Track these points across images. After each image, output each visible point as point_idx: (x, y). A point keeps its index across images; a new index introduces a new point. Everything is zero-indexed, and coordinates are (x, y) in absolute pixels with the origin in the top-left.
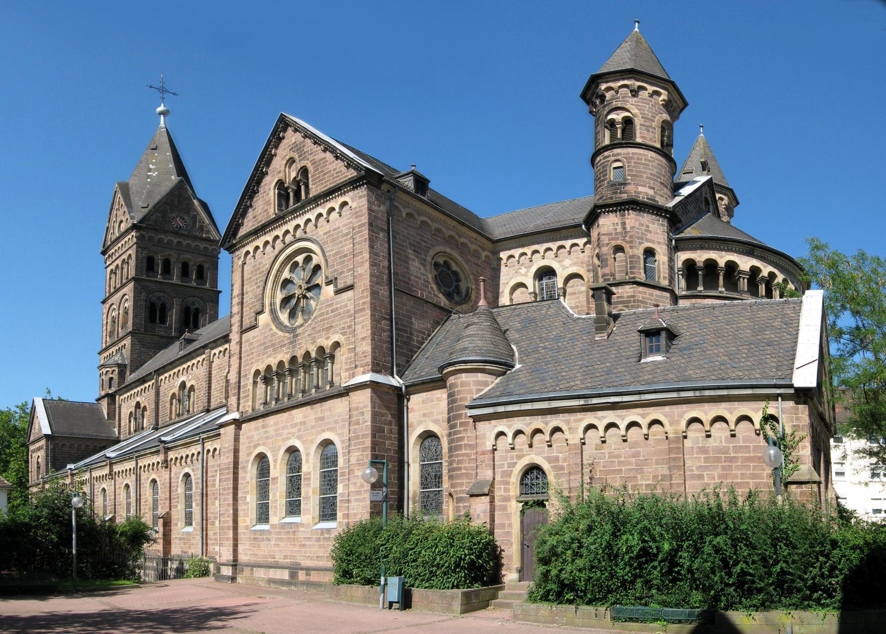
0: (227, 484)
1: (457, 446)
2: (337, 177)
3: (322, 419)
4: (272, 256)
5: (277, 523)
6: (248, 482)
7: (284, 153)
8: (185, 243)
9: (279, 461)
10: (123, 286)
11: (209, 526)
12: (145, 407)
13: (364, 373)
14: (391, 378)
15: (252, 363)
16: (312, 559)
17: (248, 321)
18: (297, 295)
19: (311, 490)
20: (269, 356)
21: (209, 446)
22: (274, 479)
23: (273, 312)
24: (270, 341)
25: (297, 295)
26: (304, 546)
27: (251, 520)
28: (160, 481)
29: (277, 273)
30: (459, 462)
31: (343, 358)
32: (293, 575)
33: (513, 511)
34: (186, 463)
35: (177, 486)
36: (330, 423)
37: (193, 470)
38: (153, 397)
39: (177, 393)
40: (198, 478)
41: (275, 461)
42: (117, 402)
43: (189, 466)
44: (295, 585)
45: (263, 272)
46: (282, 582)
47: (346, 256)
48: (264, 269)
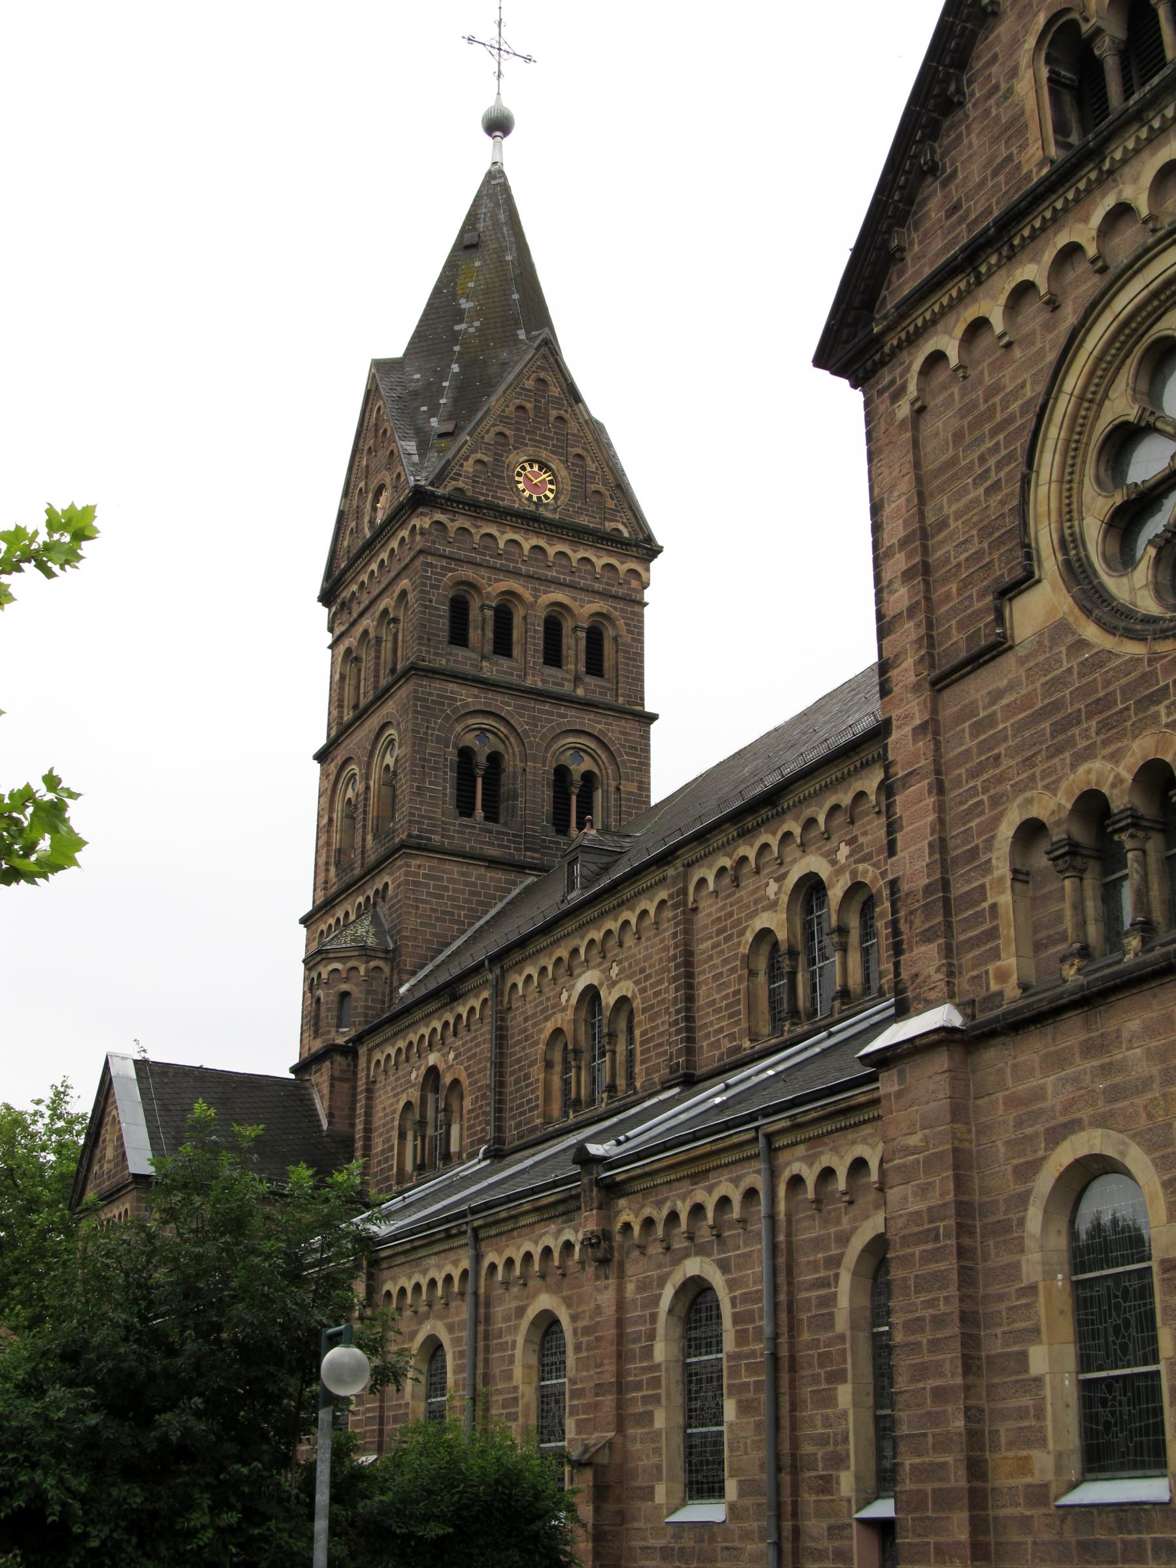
0: (931, 1303)
6: (1032, 1289)
8: (551, 551)
10: (382, 695)
11: (809, 1498)
12: (456, 1082)
15: (996, 801)
20: (1087, 754)
27: (1059, 1456)
28: (574, 1318)
29: (1078, 407)
34: (691, 1237)
35: (652, 1336)
37: (724, 1266)
38: (486, 1049)
39: (568, 1029)
42: (362, 1075)
48: (1015, 406)
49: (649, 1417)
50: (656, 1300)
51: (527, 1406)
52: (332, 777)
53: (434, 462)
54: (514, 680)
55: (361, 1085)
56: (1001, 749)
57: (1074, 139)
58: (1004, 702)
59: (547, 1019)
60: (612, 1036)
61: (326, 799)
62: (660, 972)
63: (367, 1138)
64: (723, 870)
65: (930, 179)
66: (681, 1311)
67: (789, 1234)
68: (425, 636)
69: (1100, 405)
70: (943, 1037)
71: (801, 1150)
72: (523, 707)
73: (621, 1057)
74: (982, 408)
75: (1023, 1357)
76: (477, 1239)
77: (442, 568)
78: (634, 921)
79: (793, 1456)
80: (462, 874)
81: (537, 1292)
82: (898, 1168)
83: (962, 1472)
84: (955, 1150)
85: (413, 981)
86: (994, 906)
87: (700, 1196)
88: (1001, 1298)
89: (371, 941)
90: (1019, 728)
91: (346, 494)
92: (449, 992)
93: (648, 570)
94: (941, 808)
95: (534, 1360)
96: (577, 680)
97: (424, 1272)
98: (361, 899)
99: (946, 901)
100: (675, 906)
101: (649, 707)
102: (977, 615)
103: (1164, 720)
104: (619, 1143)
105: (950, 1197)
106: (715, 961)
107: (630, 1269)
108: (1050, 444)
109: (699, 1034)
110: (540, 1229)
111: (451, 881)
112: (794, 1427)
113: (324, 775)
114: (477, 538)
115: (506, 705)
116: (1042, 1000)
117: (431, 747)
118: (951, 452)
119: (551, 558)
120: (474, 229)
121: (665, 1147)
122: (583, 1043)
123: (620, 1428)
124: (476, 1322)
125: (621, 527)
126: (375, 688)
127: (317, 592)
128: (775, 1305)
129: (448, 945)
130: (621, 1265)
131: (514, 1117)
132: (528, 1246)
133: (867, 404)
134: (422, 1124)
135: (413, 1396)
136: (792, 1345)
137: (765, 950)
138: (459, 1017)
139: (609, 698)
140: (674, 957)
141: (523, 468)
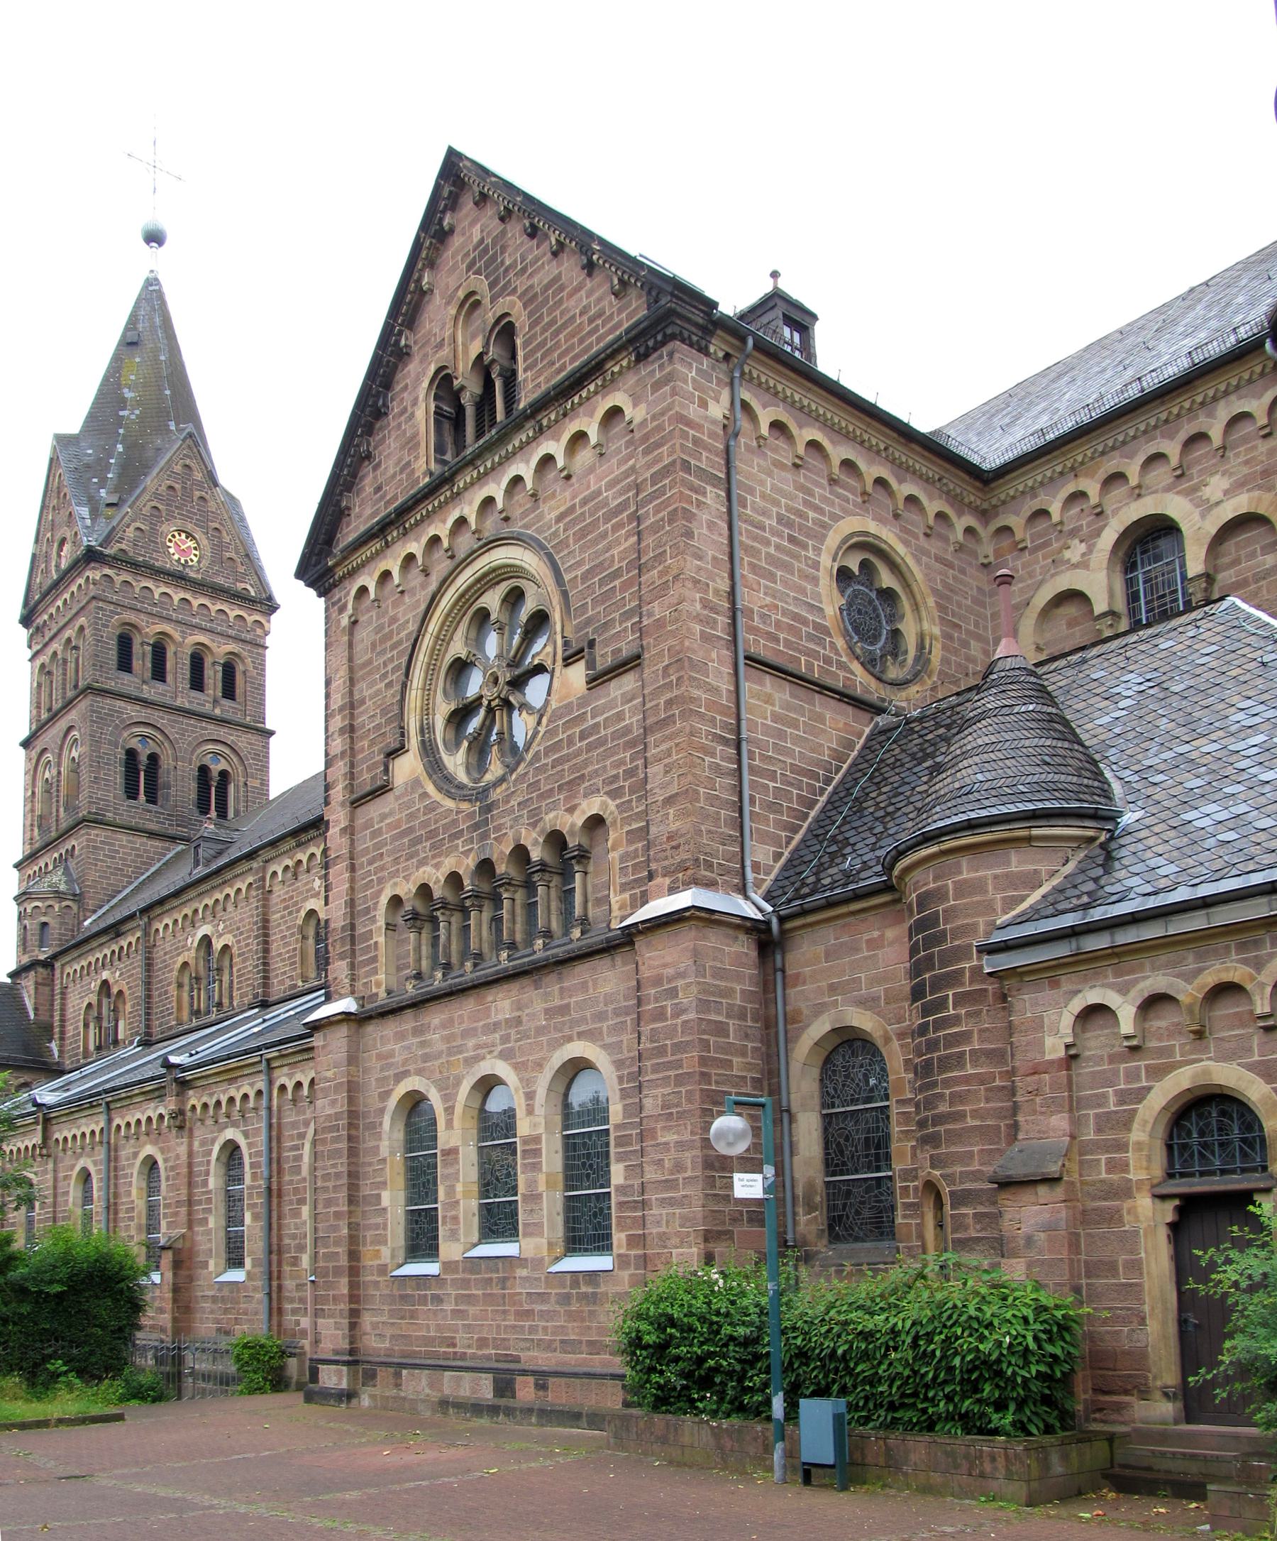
0: (334, 1166)
1: (948, 1057)
2: (590, 333)
3: (564, 1009)
4: (423, 597)
5: (458, 1257)
6: (384, 1160)
7: (452, 282)
8: (195, 603)
9: (459, 1109)
10: (68, 705)
11: (286, 1268)
12: (120, 993)
13: (672, 890)
14: (740, 899)
15: (380, 881)
16: (549, 1347)
17: (366, 776)
18: (485, 702)
19: (542, 1178)
20: (422, 863)
21: (284, 1078)
22: (447, 1153)
23: (428, 749)
24: (424, 824)
25: (485, 702)
26: (528, 1314)
27: (393, 1250)
28: (166, 1160)
29: (435, 643)
30: (956, 1098)
31: (615, 856)
32: (504, 1386)
33: (1143, 1226)
35: (207, 1173)
36: (583, 1020)
37: (246, 1134)
38: (139, 972)
39: (192, 962)
40: (258, 1154)
41: (450, 1110)
42: (57, 982)
43: (235, 1124)
44: (509, 1412)
45: (400, 643)
46: (477, 1409)
47: (616, 574)
48: (403, 634)
49: (205, 1221)
50: (209, 1152)
51: (140, 1213)
52: (34, 761)
53: (103, 528)
54: (168, 701)
55: (57, 991)
56: (384, 850)
57: (448, 457)
58: (387, 821)
59: (179, 955)
60: (219, 970)
61: (29, 777)
62: (248, 931)
63: (62, 1026)
64: (287, 867)
65: (367, 463)
66: (224, 1159)
67: (279, 1118)
68: (99, 666)
69: (448, 644)
70: (346, 1017)
71: (285, 1070)
72: (174, 721)
73: (225, 985)
74: (387, 630)
75: (379, 1196)
76: (109, 1109)
77: (111, 611)
78: (232, 895)
79: (279, 1245)
80: (129, 842)
81: (145, 1144)
82: (322, 1089)
83: (346, 1258)
84: (349, 1082)
85: (94, 917)
86: (376, 943)
87: (232, 1092)
88: (370, 1164)
89: (62, 887)
90: (394, 838)
91: (37, 541)
92: (115, 930)
93: (269, 621)
94: (352, 880)
95: (144, 1185)
96: (215, 702)
97: (79, 1127)
98: (56, 855)
99: (353, 937)
100: (258, 888)
101: (269, 726)
102: (375, 765)
103: (461, 850)
104: (191, 1055)
105: (345, 1108)
106: (283, 927)
107: (196, 1133)
108: (419, 664)
109: (272, 975)
110: (145, 1106)
111: (121, 846)
112: (279, 1229)
113: (29, 759)
114: (137, 590)
115: (161, 719)
116: (394, 1002)
117: (105, 748)
118: (369, 655)
119: (195, 609)
120: (135, 329)
121: (213, 1062)
122: (202, 972)
123: (190, 1227)
124: (109, 1161)
125: (249, 587)
126: (64, 698)
127: (17, 616)
128: (270, 1159)
129: (120, 892)
130: (191, 1130)
131: (158, 1019)
132: (138, 1115)
133: (327, 610)
134: (99, 1019)
135: (74, 1204)
136: (279, 1183)
137: (313, 922)
138: (122, 948)
139: (238, 717)
140: (256, 923)
141: (174, 536)
